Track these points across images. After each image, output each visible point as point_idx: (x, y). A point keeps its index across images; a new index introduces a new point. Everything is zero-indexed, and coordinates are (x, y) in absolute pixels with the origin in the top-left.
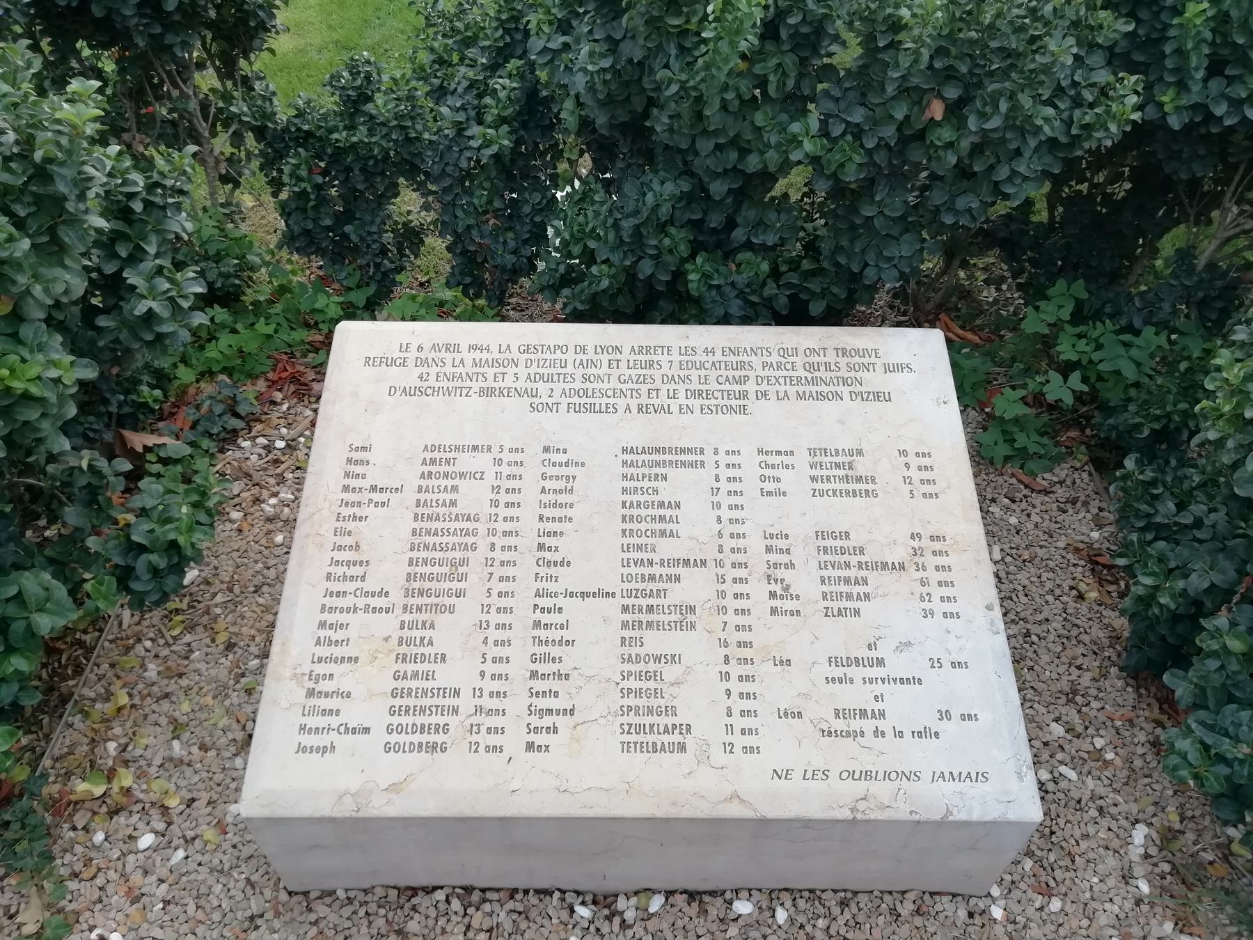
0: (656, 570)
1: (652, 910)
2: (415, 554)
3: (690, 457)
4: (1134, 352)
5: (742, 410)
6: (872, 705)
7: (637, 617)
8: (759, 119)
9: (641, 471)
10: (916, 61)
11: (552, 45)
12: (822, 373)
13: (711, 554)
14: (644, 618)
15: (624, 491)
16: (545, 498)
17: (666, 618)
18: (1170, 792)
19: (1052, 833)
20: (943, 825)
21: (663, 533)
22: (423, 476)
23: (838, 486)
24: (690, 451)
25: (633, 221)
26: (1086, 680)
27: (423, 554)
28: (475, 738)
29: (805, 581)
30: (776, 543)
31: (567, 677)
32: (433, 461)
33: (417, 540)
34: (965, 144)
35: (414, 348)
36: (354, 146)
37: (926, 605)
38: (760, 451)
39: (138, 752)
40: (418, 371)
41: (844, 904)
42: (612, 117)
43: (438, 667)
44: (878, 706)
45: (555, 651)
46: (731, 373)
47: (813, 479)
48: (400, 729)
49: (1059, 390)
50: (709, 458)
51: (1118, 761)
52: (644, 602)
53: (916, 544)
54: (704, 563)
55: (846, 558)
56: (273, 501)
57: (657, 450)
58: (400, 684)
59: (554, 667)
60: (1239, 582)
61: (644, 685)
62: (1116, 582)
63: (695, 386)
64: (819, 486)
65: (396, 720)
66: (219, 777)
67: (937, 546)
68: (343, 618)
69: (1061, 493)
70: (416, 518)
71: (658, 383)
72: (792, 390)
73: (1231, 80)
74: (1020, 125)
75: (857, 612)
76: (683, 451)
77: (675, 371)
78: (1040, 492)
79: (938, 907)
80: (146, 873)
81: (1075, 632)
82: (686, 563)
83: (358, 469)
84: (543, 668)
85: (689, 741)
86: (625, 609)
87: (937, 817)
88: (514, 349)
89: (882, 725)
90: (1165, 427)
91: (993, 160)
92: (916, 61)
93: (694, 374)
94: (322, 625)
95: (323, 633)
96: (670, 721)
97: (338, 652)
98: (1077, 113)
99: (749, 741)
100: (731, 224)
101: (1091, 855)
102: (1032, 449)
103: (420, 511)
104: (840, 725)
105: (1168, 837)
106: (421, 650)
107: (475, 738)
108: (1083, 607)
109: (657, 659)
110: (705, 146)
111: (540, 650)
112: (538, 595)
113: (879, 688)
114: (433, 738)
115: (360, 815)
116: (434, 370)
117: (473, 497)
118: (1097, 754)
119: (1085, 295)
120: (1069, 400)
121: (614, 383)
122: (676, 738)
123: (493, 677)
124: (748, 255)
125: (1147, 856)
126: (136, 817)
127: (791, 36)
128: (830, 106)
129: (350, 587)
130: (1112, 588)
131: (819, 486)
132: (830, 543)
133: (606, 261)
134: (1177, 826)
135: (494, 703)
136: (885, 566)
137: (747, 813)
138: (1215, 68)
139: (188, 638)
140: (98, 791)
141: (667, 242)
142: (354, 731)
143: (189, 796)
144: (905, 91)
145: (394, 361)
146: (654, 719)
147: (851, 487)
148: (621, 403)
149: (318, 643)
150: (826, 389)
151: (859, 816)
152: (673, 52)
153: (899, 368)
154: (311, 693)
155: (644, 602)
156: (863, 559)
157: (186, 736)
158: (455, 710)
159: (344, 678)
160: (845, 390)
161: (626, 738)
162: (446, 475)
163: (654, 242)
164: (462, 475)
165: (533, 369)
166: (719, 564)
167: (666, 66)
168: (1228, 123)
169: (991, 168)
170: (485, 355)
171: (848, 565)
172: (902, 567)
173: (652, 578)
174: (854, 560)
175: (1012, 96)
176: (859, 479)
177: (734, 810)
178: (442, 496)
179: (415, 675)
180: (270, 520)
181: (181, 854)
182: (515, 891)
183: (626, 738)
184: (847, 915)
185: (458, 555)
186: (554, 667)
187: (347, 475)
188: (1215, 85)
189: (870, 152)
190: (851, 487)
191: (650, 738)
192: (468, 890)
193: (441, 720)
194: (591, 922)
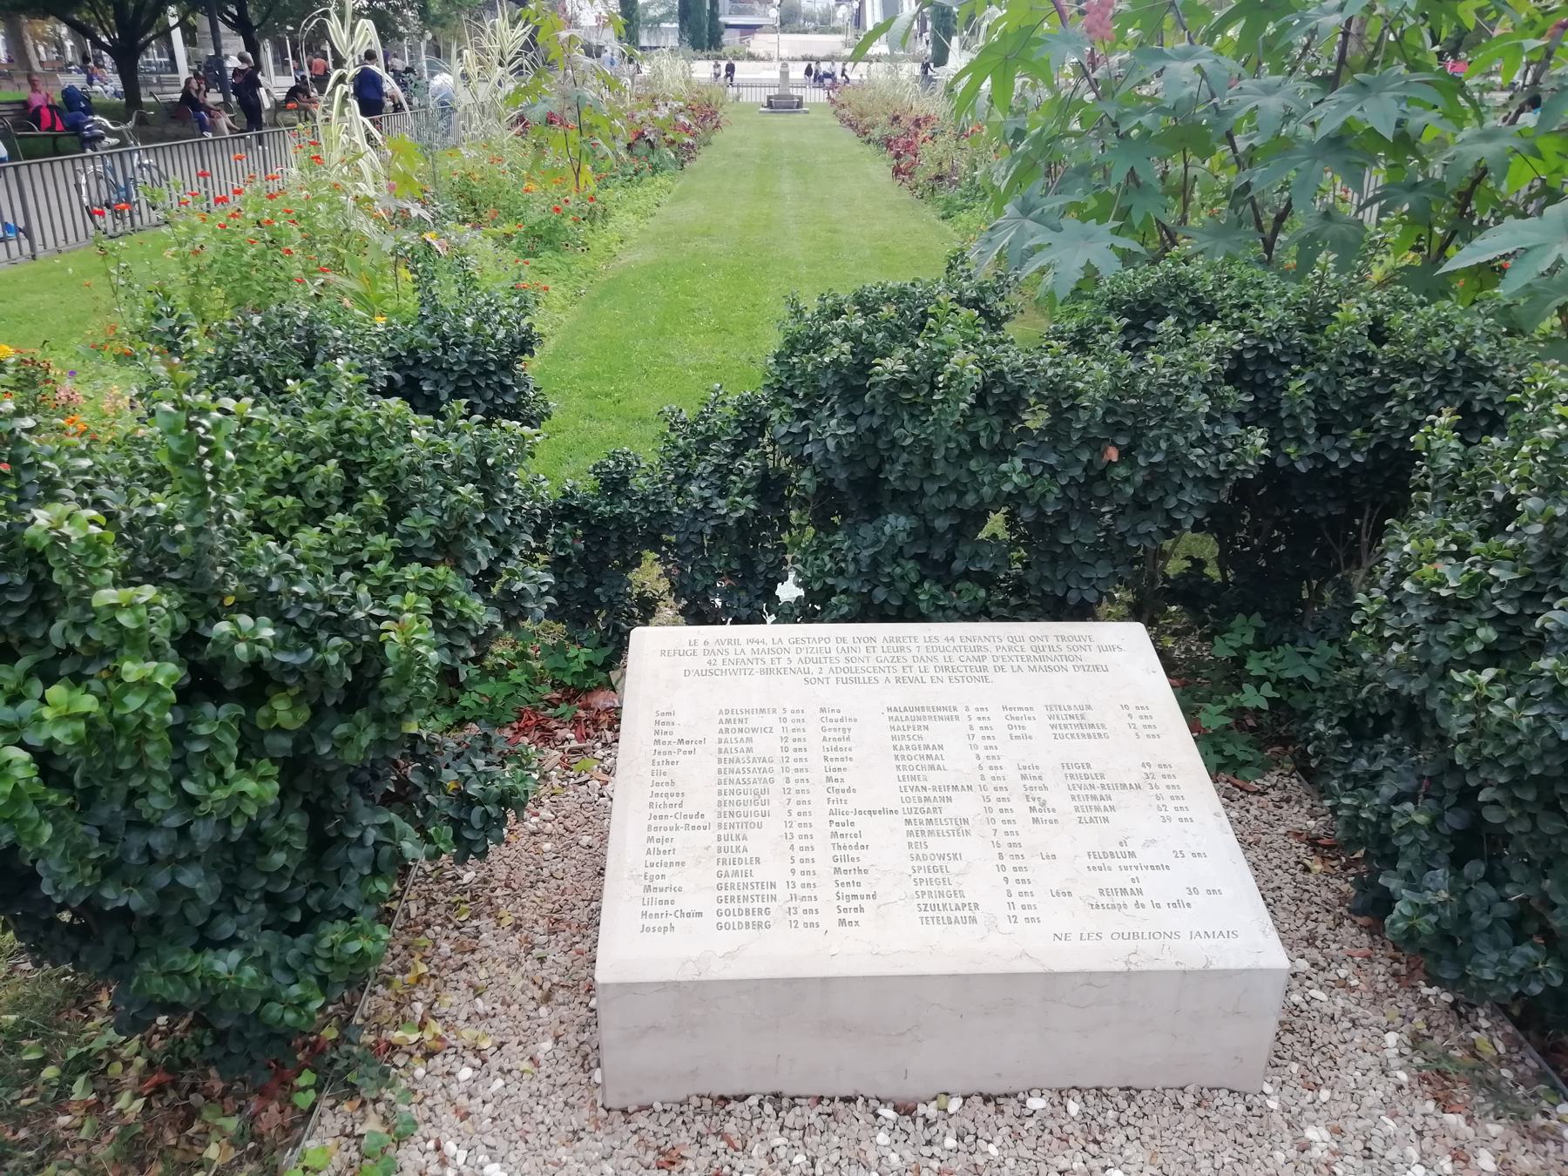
0: (930, 794)
1: (951, 1111)
2: (723, 787)
3: (947, 713)
4: (1312, 660)
5: (985, 679)
6: (1129, 886)
7: (919, 827)
8: (973, 465)
9: (905, 724)
10: (1092, 417)
11: (794, 430)
12: (1047, 652)
13: (975, 781)
14: (925, 828)
15: (893, 738)
16: (828, 745)
17: (944, 828)
18: (1414, 1008)
19: (1312, 1042)
20: (1206, 976)
21: (932, 767)
22: (721, 731)
23: (1074, 731)
24: (945, 709)
25: (871, 551)
26: (1322, 929)
27: (729, 787)
28: (793, 917)
29: (1059, 798)
30: (1028, 772)
31: (866, 871)
32: (728, 721)
33: (723, 777)
34: (1138, 479)
35: (700, 642)
36: (617, 517)
37: (1163, 813)
38: (1004, 708)
39: (444, 1009)
40: (707, 658)
41: (1130, 1099)
42: (852, 474)
43: (754, 867)
44: (1134, 886)
45: (853, 853)
46: (970, 655)
47: (1053, 727)
48: (728, 913)
49: (1252, 698)
50: (961, 712)
51: (1362, 986)
52: (924, 817)
53: (1147, 770)
54: (970, 788)
55: (1090, 781)
56: (535, 819)
57: (917, 709)
58: (723, 880)
59: (855, 865)
60: (1419, 787)
61: (933, 876)
62: (1338, 858)
63: (941, 663)
64: (1058, 731)
65: (723, 906)
66: (526, 1024)
67: (1166, 771)
68: (668, 834)
69: (1275, 794)
70: (720, 761)
71: (910, 662)
72: (1024, 665)
73: (1338, 437)
74: (1175, 458)
75: (1106, 820)
76: (939, 709)
77: (924, 654)
78: (1254, 793)
79: (1218, 1102)
80: (470, 1097)
81: (1306, 896)
82: (955, 788)
83: (665, 728)
84: (844, 866)
85: (978, 914)
86: (908, 822)
87: (1199, 966)
88: (786, 642)
89: (1141, 899)
90: (1352, 715)
91: (1162, 494)
92: (1092, 417)
93: (940, 656)
94: (650, 839)
95: (652, 846)
96: (960, 901)
97: (667, 858)
98: (1222, 457)
99: (1030, 913)
100: (951, 557)
101: (1350, 1056)
102: (1241, 757)
103: (722, 756)
104: (1105, 900)
105: (1417, 1041)
106: (737, 856)
107: (793, 917)
108: (1311, 877)
109: (942, 857)
110: (931, 488)
111: (839, 853)
112: (831, 813)
113: (1134, 873)
114: (757, 918)
115: (703, 978)
116: (719, 658)
117: (765, 745)
118: (1344, 984)
119: (1263, 624)
120: (1265, 706)
121: (873, 663)
122: (966, 913)
123: (803, 873)
124: (967, 584)
125: (1401, 1055)
126: (450, 1058)
127: (996, 403)
128: (1028, 454)
129: (670, 812)
130: (1335, 863)
131: (1058, 731)
132: (1074, 771)
133: (844, 592)
134: (1425, 1032)
135: (806, 892)
136: (1124, 786)
137: (1038, 969)
138: (1323, 429)
139: (475, 923)
140: (414, 1037)
141: (898, 570)
142: (689, 915)
143: (499, 1040)
144: (1086, 441)
145: (685, 653)
146: (946, 900)
147: (1085, 731)
148: (881, 676)
149: (649, 852)
150: (1052, 664)
151: (1133, 968)
152: (906, 417)
153: (1112, 648)
154: (648, 889)
155: (924, 817)
156: (1105, 782)
157: (487, 995)
158: (774, 898)
159: (674, 877)
160: (1069, 665)
161: (925, 914)
162: (741, 730)
163: (888, 570)
164: (754, 730)
165: (803, 654)
166: (984, 788)
167: (902, 426)
168: (1342, 466)
169: (1161, 500)
170: (761, 646)
171: (1092, 787)
172: (1138, 787)
173: (927, 799)
174: (1097, 783)
175: (1169, 438)
176: (1092, 726)
177: (1023, 966)
178: (739, 746)
179: (736, 873)
180: (533, 834)
181: (500, 1083)
182: (822, 1098)
183: (925, 914)
184: (1134, 1108)
185: (759, 786)
186: (855, 865)
187: (657, 732)
188: (1326, 442)
189: (1063, 488)
190: (1085, 731)
191: (945, 914)
192: (777, 1096)
193: (763, 906)
194: (896, 1123)
